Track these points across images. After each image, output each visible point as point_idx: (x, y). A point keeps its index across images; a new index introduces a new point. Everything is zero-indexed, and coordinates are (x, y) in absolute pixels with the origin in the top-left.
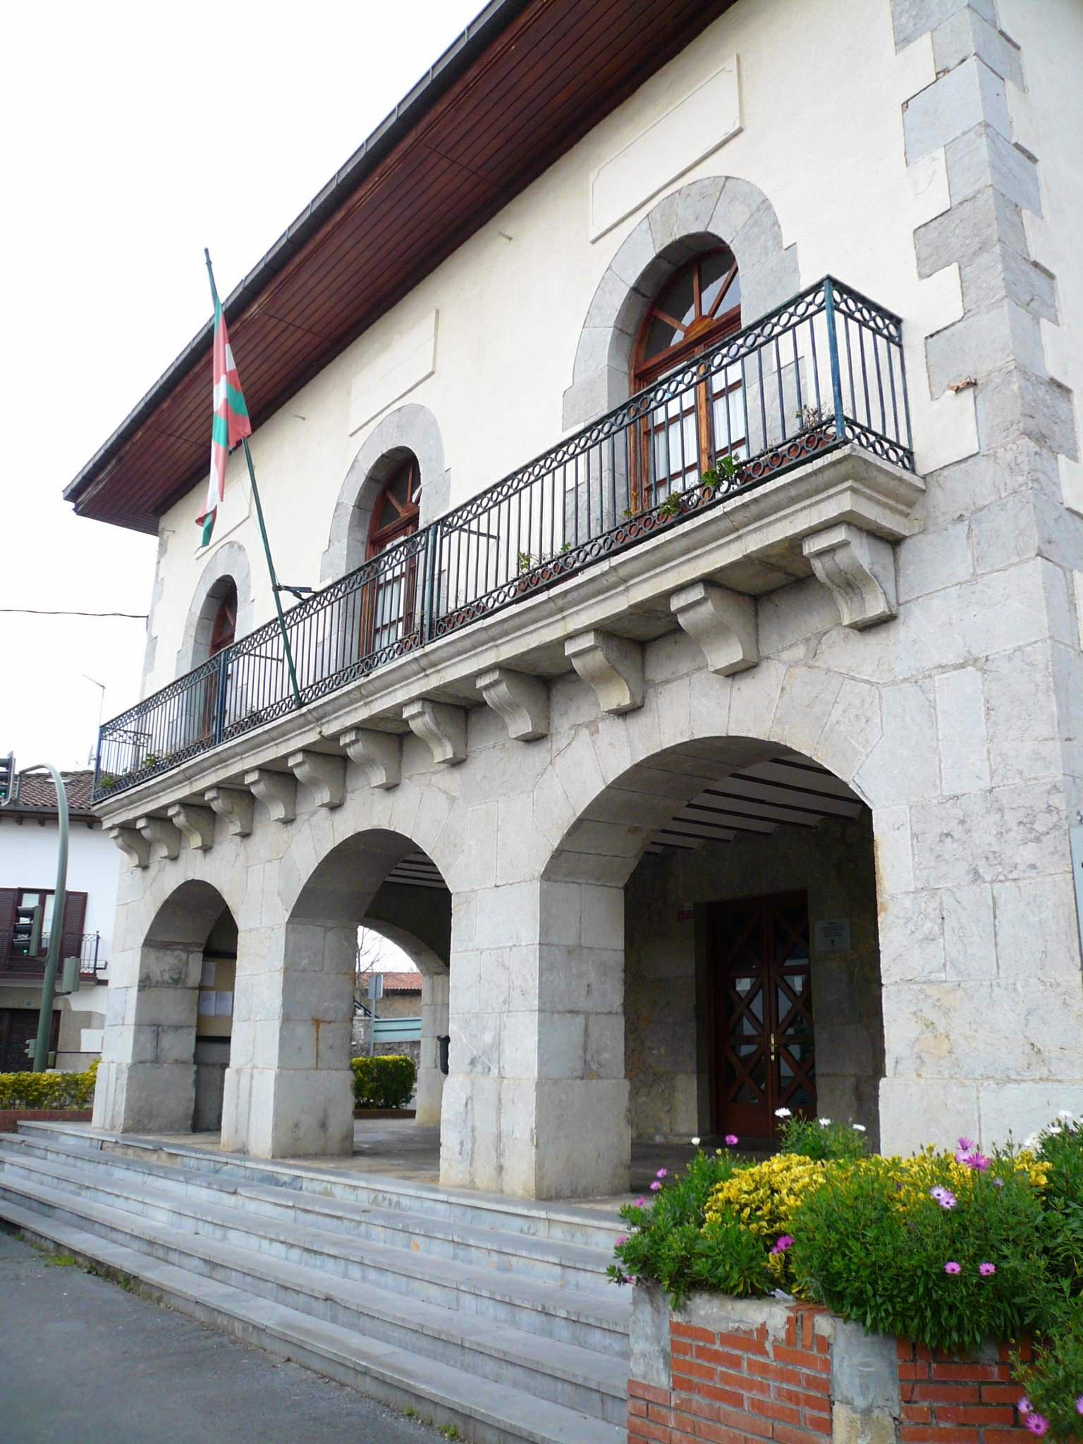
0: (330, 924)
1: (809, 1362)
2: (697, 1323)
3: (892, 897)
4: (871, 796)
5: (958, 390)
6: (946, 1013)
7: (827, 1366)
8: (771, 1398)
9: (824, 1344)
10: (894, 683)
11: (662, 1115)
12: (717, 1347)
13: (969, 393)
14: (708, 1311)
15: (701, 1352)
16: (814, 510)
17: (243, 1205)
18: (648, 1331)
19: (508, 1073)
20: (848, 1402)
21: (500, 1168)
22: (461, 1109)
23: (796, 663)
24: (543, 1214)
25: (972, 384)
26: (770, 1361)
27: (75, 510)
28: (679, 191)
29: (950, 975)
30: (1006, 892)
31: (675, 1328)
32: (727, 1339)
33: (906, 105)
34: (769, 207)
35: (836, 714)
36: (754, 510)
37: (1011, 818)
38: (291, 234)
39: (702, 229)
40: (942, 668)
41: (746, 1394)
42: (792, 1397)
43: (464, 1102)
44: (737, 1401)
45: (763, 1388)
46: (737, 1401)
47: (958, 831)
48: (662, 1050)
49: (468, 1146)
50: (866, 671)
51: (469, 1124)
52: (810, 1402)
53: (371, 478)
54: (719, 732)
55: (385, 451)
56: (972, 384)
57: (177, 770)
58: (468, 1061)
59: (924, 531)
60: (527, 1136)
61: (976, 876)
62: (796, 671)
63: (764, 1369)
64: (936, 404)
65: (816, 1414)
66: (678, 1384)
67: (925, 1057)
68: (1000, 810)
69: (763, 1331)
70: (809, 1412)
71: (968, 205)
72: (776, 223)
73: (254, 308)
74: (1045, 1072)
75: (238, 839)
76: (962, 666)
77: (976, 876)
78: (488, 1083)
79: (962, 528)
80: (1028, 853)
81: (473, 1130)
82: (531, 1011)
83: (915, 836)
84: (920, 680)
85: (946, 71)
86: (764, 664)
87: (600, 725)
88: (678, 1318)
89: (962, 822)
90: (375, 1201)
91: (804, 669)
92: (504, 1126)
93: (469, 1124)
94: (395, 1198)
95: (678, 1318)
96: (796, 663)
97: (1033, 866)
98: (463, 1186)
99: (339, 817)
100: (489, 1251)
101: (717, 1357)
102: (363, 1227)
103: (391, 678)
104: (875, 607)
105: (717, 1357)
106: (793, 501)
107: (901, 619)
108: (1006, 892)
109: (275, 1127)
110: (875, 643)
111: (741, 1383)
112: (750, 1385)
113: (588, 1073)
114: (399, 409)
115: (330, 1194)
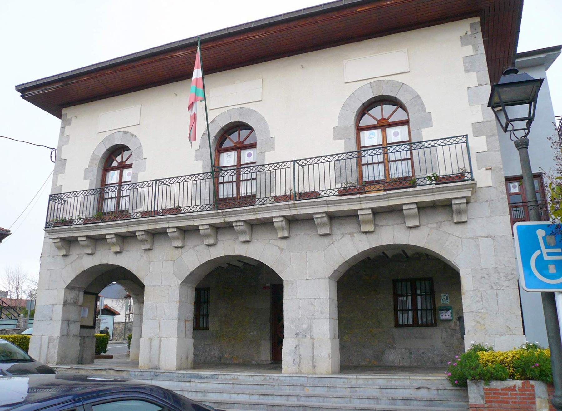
0: (190, 285)
1: (529, 390)
2: (492, 387)
3: (467, 291)
4: (459, 265)
5: (487, 169)
6: (483, 319)
7: (534, 391)
8: (518, 400)
9: (533, 386)
10: (466, 238)
11: (254, 354)
12: (500, 391)
13: (489, 171)
14: (496, 384)
15: (494, 394)
16: (459, 193)
17: (196, 386)
18: (475, 391)
19: (315, 337)
20: (540, 397)
21: (314, 366)
22: (294, 349)
23: (433, 228)
24: (355, 377)
25: (491, 169)
26: (518, 392)
27: (21, 96)
28: (384, 80)
29: (484, 310)
30: (500, 292)
31: (486, 389)
32: (502, 389)
33: (468, 88)
34: (420, 98)
35: (447, 244)
36: (441, 189)
37: (502, 275)
38: (213, 36)
39: (394, 95)
40: (481, 237)
41: (510, 401)
42: (524, 399)
43: (295, 346)
44: (508, 402)
45: (515, 398)
46: (508, 402)
47: (486, 277)
48: (255, 333)
49: (297, 360)
50: (457, 234)
51: (298, 353)
52: (529, 399)
53: (223, 129)
54: (392, 243)
55: (233, 121)
56: (491, 169)
57: (123, 222)
58: (294, 333)
59: (475, 202)
60: (327, 356)
61: (492, 288)
62: (433, 230)
63: (516, 394)
64: (479, 171)
65: (531, 401)
66: (487, 402)
67: (478, 330)
68: (499, 273)
69: (515, 386)
70: (529, 401)
71: (488, 123)
72: (422, 104)
73: (180, 53)
74: (511, 333)
75: (143, 251)
76: (487, 237)
77: (492, 288)
78: (307, 340)
79: (487, 204)
80: (506, 283)
81: (300, 355)
82: (326, 318)
83: (473, 277)
84: (475, 239)
85: (481, 85)
86: (421, 227)
87: (355, 235)
88: (486, 387)
89: (488, 275)
90: (265, 379)
91: (436, 230)
92: (315, 353)
93: (298, 353)
94: (277, 378)
95: (486, 387)
96: (433, 228)
97: (508, 286)
98: (296, 373)
99: (212, 249)
100: (346, 388)
101: (500, 394)
102: (277, 387)
103: (271, 208)
104: (464, 219)
105: (500, 394)
106: (453, 189)
107: (468, 223)
108: (500, 292)
109: (177, 358)
110: (460, 227)
111: (509, 398)
112: (511, 398)
113: (335, 338)
114: (241, 108)
115: (237, 379)
